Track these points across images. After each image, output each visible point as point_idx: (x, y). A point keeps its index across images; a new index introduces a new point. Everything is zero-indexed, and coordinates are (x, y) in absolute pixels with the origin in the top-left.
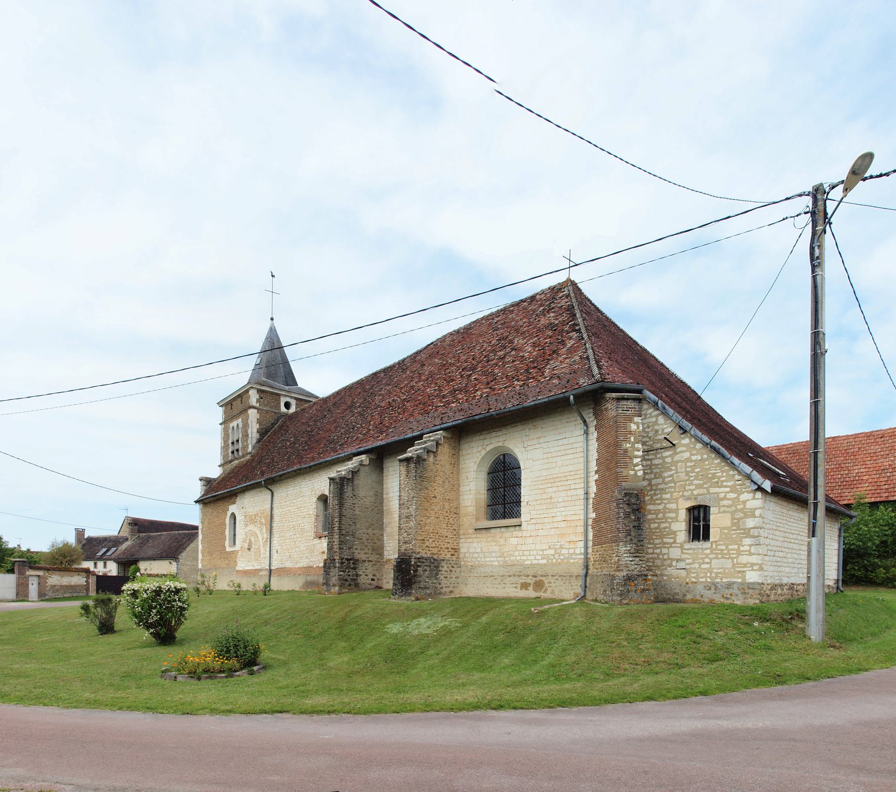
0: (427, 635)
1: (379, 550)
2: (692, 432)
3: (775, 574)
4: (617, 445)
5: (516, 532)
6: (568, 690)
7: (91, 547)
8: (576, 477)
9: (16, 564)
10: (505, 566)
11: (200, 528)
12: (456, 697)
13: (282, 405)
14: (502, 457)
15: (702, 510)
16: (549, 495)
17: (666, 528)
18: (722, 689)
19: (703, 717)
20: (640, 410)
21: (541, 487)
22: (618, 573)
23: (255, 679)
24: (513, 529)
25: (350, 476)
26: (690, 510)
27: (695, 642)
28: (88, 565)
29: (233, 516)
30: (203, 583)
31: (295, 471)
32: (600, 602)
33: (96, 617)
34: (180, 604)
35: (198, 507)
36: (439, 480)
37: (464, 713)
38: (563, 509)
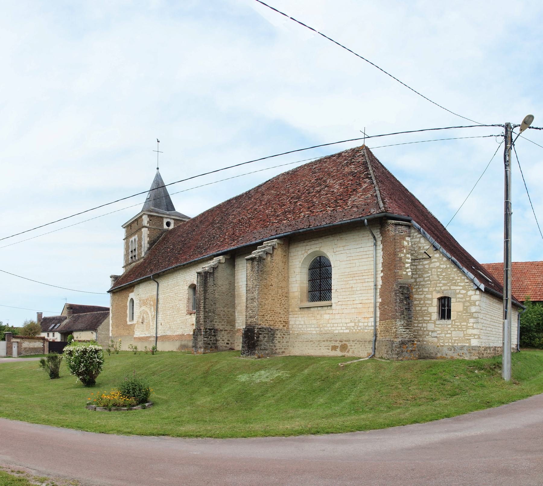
0: (266, 383)
1: (232, 322)
2: (441, 250)
3: (486, 341)
4: (395, 254)
5: (328, 311)
6: (363, 419)
7: (46, 323)
8: (369, 274)
9: (6, 335)
10: (321, 334)
11: (111, 309)
12: (286, 426)
13: (165, 224)
14: (318, 258)
15: (446, 300)
16: (351, 286)
17: (425, 310)
18: (458, 413)
19: (447, 432)
20: (410, 233)
21: (345, 279)
22: (396, 340)
23: (146, 412)
24: (326, 308)
25: (212, 271)
26: (440, 299)
27: (442, 384)
28: (44, 335)
29: (132, 300)
30: (113, 346)
31: (173, 268)
32: (384, 359)
33: (49, 367)
34: (98, 360)
35: (109, 295)
36: (275, 273)
37: (292, 437)
38: (360, 295)
